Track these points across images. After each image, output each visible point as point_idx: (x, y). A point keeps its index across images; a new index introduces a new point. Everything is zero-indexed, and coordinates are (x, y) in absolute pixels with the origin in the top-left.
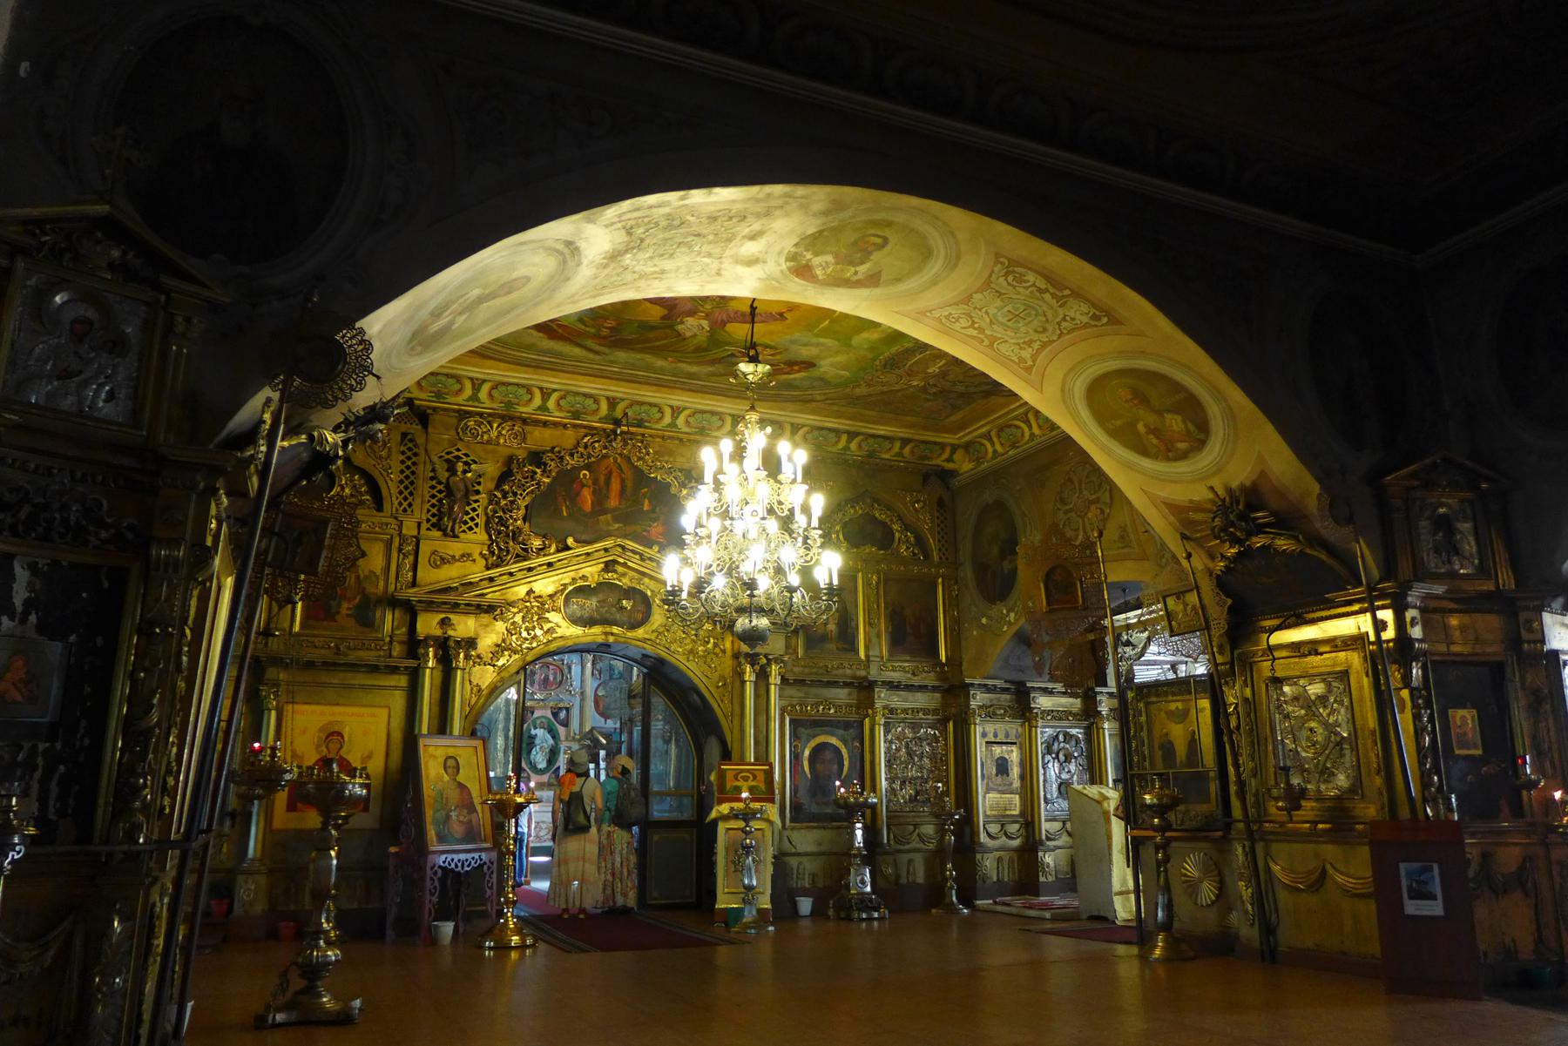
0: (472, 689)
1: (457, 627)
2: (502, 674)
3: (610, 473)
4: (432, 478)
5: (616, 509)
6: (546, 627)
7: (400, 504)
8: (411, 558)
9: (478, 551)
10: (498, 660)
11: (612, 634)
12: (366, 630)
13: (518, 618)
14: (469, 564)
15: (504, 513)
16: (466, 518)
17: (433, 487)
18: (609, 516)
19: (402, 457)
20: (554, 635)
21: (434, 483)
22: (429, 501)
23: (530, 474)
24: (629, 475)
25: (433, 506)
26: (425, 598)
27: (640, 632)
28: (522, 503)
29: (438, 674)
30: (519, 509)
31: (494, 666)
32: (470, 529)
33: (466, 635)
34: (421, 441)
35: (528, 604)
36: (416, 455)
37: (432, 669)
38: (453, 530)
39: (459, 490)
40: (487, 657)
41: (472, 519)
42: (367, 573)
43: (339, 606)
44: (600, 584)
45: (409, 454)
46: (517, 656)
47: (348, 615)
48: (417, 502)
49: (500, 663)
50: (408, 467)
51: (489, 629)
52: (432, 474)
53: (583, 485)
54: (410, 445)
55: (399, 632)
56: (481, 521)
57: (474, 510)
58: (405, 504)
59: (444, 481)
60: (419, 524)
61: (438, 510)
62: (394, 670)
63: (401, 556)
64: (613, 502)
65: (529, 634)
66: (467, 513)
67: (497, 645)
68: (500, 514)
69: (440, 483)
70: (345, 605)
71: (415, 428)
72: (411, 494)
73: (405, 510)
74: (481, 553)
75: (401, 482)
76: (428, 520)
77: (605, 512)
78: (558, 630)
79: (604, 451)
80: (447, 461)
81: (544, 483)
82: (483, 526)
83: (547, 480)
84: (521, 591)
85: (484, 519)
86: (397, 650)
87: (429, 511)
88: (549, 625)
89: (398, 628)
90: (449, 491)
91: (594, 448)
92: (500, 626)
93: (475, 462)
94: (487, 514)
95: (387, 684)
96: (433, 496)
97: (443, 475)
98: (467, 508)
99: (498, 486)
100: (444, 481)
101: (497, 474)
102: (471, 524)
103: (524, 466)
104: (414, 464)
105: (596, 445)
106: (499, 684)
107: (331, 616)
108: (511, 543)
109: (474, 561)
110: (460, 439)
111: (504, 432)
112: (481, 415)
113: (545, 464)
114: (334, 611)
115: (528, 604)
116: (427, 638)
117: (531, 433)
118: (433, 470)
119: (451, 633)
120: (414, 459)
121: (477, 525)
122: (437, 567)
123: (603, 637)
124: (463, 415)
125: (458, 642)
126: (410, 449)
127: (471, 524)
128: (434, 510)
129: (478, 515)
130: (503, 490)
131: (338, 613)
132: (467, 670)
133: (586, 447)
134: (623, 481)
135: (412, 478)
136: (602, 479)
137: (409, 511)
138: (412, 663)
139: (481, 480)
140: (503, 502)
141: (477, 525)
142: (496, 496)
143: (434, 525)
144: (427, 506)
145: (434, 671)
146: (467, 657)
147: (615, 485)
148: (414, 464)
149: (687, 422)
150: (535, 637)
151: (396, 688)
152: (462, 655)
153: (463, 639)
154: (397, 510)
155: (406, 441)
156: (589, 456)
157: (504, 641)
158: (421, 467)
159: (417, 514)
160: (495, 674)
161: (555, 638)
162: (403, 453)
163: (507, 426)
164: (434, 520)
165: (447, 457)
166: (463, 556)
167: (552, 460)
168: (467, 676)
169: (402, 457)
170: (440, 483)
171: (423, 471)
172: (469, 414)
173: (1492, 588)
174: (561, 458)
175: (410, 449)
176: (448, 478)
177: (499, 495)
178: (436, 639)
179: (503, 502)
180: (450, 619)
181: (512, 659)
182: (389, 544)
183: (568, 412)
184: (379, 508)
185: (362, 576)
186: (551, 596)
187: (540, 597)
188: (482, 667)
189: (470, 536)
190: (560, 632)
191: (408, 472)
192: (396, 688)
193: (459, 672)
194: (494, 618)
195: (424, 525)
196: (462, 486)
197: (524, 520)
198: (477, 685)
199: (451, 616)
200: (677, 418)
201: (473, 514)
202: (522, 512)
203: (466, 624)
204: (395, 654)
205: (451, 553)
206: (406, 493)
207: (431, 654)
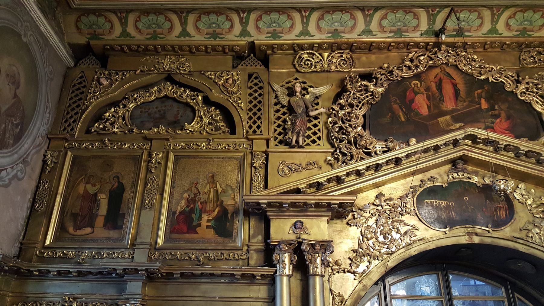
0: (334, 299)
1: (311, 231)
2: (364, 282)
3: (441, 80)
4: (276, 104)
5: (453, 111)
6: (403, 229)
7: (250, 127)
8: (262, 171)
9: (324, 158)
10: (358, 267)
11: (476, 234)
12: (226, 240)
13: (372, 222)
14: (315, 171)
15: (344, 123)
16: (308, 133)
17: (277, 111)
18: (448, 117)
19: (249, 91)
20: (413, 238)
21: (278, 107)
22: (275, 123)
23: (363, 88)
24: (459, 79)
25: (279, 126)
26: (275, 199)
27: (507, 231)
28: (361, 113)
29: (296, 282)
30: (357, 118)
31: (354, 273)
32: (314, 142)
33: (320, 238)
34: (264, 77)
35: (380, 208)
36: (261, 88)
37: (290, 276)
38: (297, 142)
39: (299, 106)
40: (345, 264)
41: (315, 133)
42: (224, 186)
43: (200, 218)
44: (450, 184)
45: (255, 88)
46: (377, 262)
47: (208, 227)
48: (265, 123)
49: (360, 270)
50: (255, 98)
51: (343, 234)
52: (276, 100)
53: (416, 93)
54: (256, 81)
55: (255, 240)
56: (323, 134)
57: (315, 126)
58: (254, 127)
59: (286, 104)
60: (267, 141)
61: (282, 129)
62: (250, 279)
63: (253, 169)
64: (449, 105)
65: (385, 238)
66: (309, 129)
67: (354, 251)
68: (340, 124)
69: (283, 107)
70: (205, 217)
71: (259, 68)
72: (259, 118)
73: (255, 132)
74: (326, 160)
75: (250, 110)
76: (276, 138)
77: (443, 114)
78: (416, 232)
79: (431, 62)
80: (288, 88)
81: (378, 92)
82: (325, 138)
83: (381, 90)
84: (371, 195)
85: (325, 132)
86: (255, 258)
87: (275, 130)
88: (406, 228)
89: (254, 236)
90: (291, 110)
91: (420, 61)
92: (354, 232)
93: (311, 87)
94: (327, 128)
95: (247, 295)
96: (279, 118)
97: (284, 99)
98: (309, 125)
99: (335, 102)
100: (286, 104)
101: (332, 95)
102: (314, 137)
103: (357, 82)
104: (260, 95)
105: (422, 58)
106: (363, 293)
107: (192, 229)
108: (354, 148)
109: (320, 168)
110: (298, 71)
111: (334, 61)
112: (311, 46)
113: (377, 79)
114: (195, 224)
115: (380, 208)
116: (280, 243)
117: (359, 59)
118: (276, 97)
119: (304, 236)
120: (260, 91)
121: (319, 138)
122: (285, 175)
123: (466, 237)
124: (296, 48)
125: (312, 246)
126: (256, 84)
127: (314, 137)
128: (280, 130)
129: (319, 130)
130: (340, 104)
131: (199, 225)
132: (326, 278)
133: (412, 60)
134: (455, 85)
135: (259, 106)
136: (433, 85)
137: (258, 131)
138: (268, 271)
139: (319, 101)
140: (341, 113)
141: (319, 138)
142: (333, 109)
143: (281, 142)
144: (274, 126)
145: (292, 279)
146: (325, 264)
147: (448, 89)
148: (260, 102)
149: (508, 25)
150: (393, 241)
151: (255, 299)
152: (319, 261)
153: (317, 242)
154: (247, 132)
155: (252, 79)
156: (417, 67)
157: (360, 246)
158: (266, 97)
159: (265, 132)
160: (357, 282)
161: (415, 241)
162: (251, 88)
163: (336, 54)
164: (280, 138)
165: (287, 85)
166: (309, 164)
167: (382, 75)
168: (326, 285)
169: (249, 91)
170: (283, 107)
171: (268, 100)
172: (301, 47)
173: (476, 281)
174: (391, 72)
175: (256, 84)
176: (289, 102)
177: (337, 108)
178: (289, 243)
179: (341, 113)
180: (302, 223)
181: (373, 265)
182: (242, 161)
183: (390, 32)
184: (233, 131)
185: (220, 190)
186: (401, 198)
187: (391, 199)
188: (342, 274)
189: (314, 147)
190: (420, 234)
191: (255, 102)
192: (255, 299)
193: (318, 279)
194: (348, 224)
195: (272, 143)
196: (302, 104)
197: (364, 127)
198: (339, 295)
199: (304, 220)
200: (497, 22)
201: (316, 129)
202: (360, 121)
203: (319, 227)
204: (252, 262)
205: (298, 163)
206: (255, 118)
207: (287, 261)
